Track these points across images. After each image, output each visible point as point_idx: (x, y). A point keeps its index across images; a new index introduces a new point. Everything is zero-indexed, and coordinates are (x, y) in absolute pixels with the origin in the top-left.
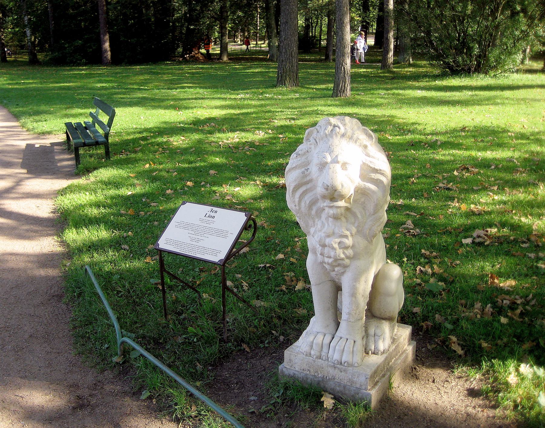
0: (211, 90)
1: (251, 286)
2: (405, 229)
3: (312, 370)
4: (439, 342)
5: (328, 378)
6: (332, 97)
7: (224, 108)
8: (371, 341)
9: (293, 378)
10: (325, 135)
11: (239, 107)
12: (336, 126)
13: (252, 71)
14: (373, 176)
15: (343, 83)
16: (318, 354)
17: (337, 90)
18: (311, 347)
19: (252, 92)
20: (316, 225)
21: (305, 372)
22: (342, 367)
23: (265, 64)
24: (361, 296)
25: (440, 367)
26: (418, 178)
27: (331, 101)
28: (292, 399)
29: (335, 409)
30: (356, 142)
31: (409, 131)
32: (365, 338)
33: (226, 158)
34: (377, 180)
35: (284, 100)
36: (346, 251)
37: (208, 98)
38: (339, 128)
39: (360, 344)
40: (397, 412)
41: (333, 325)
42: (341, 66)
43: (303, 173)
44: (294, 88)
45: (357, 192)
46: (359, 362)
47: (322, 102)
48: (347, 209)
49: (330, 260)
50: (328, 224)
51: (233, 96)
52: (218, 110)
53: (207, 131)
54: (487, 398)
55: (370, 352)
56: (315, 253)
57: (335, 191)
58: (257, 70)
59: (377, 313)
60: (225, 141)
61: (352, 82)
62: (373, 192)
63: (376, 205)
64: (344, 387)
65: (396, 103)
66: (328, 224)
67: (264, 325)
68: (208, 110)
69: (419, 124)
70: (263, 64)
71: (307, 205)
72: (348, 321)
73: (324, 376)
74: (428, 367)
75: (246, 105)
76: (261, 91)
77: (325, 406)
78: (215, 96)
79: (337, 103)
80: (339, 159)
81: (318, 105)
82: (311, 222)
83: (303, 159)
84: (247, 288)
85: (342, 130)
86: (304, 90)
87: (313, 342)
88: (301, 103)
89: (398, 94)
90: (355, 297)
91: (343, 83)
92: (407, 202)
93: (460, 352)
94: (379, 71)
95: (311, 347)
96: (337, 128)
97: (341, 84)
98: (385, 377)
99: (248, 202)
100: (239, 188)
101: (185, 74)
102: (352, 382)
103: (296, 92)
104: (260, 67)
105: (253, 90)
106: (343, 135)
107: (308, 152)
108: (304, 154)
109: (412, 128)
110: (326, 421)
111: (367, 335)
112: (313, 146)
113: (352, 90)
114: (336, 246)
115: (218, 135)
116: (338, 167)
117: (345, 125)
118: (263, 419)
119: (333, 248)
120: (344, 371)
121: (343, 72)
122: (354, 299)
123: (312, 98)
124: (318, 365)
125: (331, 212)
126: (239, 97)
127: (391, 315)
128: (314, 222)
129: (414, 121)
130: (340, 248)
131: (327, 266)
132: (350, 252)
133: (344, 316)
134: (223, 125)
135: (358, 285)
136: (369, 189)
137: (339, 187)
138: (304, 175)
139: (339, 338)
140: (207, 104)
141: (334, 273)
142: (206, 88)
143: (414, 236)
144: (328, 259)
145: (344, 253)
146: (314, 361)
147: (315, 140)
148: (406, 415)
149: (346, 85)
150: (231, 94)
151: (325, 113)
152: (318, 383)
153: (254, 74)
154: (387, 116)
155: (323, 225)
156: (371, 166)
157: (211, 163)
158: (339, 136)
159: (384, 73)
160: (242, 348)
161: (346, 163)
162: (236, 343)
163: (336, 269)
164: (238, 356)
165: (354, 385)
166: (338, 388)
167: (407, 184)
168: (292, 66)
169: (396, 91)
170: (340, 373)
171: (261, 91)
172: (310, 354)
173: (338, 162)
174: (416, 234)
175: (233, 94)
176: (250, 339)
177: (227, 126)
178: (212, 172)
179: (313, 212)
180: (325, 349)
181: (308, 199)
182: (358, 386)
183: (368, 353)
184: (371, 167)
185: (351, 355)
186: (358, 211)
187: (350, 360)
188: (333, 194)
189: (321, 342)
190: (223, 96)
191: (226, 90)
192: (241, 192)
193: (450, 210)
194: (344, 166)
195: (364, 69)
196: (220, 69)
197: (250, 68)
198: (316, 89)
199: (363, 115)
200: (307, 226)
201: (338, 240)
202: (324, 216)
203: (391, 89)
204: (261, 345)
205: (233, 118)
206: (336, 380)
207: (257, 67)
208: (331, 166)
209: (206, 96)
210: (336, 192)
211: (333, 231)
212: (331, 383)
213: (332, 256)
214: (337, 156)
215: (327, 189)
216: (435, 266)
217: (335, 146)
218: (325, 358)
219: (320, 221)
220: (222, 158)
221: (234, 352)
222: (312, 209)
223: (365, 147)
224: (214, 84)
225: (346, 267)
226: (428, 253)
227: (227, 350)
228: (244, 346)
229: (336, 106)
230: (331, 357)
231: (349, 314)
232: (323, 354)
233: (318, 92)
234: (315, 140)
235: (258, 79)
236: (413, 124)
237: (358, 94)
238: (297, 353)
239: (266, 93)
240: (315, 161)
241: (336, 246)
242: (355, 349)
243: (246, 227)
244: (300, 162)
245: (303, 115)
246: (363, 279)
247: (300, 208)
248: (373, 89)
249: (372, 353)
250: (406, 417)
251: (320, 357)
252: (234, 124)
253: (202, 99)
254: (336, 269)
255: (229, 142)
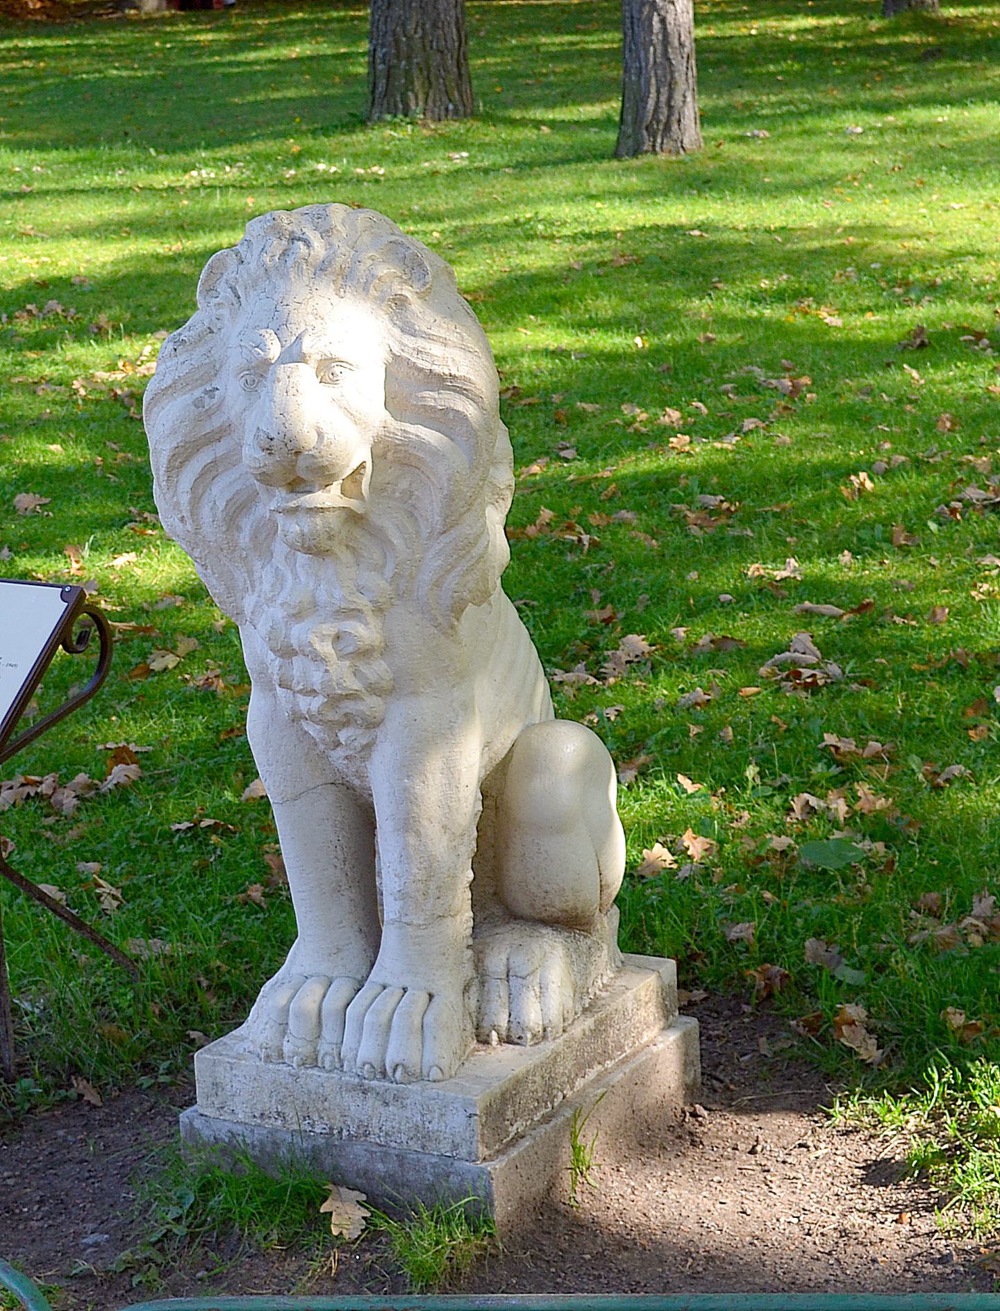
0: (65, 154)
1: (129, 894)
2: (781, 666)
3: (290, 1114)
4: (801, 1030)
5: (345, 1133)
6: (616, 155)
7: (114, 232)
8: (494, 996)
9: (230, 1149)
10: (262, 271)
11: (184, 227)
12: (299, 239)
13: (271, 53)
14: (432, 398)
15: (664, 90)
16: (306, 1050)
17: (637, 121)
18: (283, 1028)
19: (255, 157)
20: (257, 584)
21: (269, 1124)
22: (387, 1084)
23: (340, 20)
24: (438, 827)
25: (789, 1109)
26: (887, 474)
27: (607, 174)
28: (226, 1222)
29: (371, 1234)
30: (366, 289)
31: (932, 288)
32: (474, 989)
33: (92, 445)
34: (446, 411)
35: (393, 184)
36: (363, 668)
37: (47, 193)
38: (308, 243)
39: (450, 1003)
40: (594, 1243)
41: (355, 946)
42: (646, 10)
43: (198, 403)
44: (454, 127)
45: (384, 456)
46: (444, 1063)
47: (561, 181)
48: (353, 518)
49: (316, 703)
50: (296, 576)
51: (162, 180)
52: (85, 242)
53: (27, 336)
54: (923, 1179)
55: (494, 1034)
56: (268, 687)
57: (298, 453)
58: (296, 51)
59: (524, 908)
60: (102, 375)
61: (703, 85)
62: (435, 453)
63: (450, 498)
64: (401, 1158)
65: (904, 167)
66: (296, 576)
67: (162, 1016)
68: (38, 248)
69: (979, 255)
70: (330, 20)
71: (219, 515)
72: (402, 923)
73: (332, 1129)
74: (741, 1111)
75: (216, 214)
76: (296, 149)
77: (335, 1232)
78: (82, 182)
79: (634, 181)
80: (306, 346)
81: (544, 198)
82: (240, 577)
83: (197, 356)
84: (115, 903)
85: (319, 247)
86: (492, 133)
87: (286, 1009)
88: (465, 196)
89: (928, 129)
90: (418, 834)
91: (664, 90)
92: (818, 567)
93: (870, 1051)
94: (875, 24)
95: (283, 1028)
96: (301, 244)
97: (653, 95)
98: (552, 1124)
99: (161, 607)
100: (132, 556)
101: (845, 49)
102: (425, 1137)
103: (459, 145)
104: (314, 34)
105: (259, 146)
106: (322, 268)
107: (212, 332)
108: (201, 337)
109: (948, 274)
110: (335, 1280)
111: (481, 975)
112: (225, 312)
113: (706, 119)
114: (326, 648)
115: (74, 351)
116: (304, 375)
117: (326, 233)
118: (120, 1293)
119: (317, 658)
120: (396, 1098)
121: (657, 38)
122: (412, 840)
123: (523, 168)
124: (310, 1092)
125: (294, 527)
126: (193, 177)
127: (571, 904)
128: (250, 572)
129: (960, 242)
130: (340, 658)
131: (312, 729)
132: (378, 669)
133: (390, 908)
134: (99, 309)
135: (419, 789)
136: (421, 444)
137: (309, 439)
138: (202, 410)
139: (379, 988)
140: (41, 220)
141: (340, 752)
142: (41, 146)
143: (812, 688)
144: (308, 699)
145: (356, 673)
146: (296, 1077)
147: (233, 289)
148: (626, 1249)
149: (678, 98)
150: (154, 168)
151: (566, 231)
152: (315, 1155)
153: (282, 71)
154: (846, 229)
155: (278, 576)
156: (421, 364)
157: (27, 465)
158: (308, 272)
159: (895, 31)
160: (72, 1093)
161: (332, 360)
162: (48, 1079)
163: (343, 736)
164: (58, 1120)
165: (431, 1146)
166: (380, 1166)
167: (834, 499)
168: (434, 26)
169: (921, 115)
170: (382, 1109)
171: (294, 146)
172: (281, 1055)
173: (302, 358)
174: (821, 682)
175: (165, 167)
176: (103, 1060)
177: (116, 311)
178: (25, 500)
179: (244, 538)
180: (329, 1034)
181: (220, 493)
182: (446, 1149)
183: (486, 1042)
184: (421, 370)
185: (415, 1041)
186: (389, 522)
187: (413, 1059)
188: (293, 466)
189: (314, 1007)
190: (117, 178)
191: (132, 153)
192: (138, 572)
193: (985, 587)
194: (328, 369)
195: (807, 15)
196: (122, 53)
197: (268, 38)
198: (553, 124)
199: (735, 229)
200: (230, 589)
201: (330, 629)
202: (280, 548)
203: (900, 105)
204: (145, 1081)
205: (148, 276)
206: (372, 1138)
207: (300, 37)
208: (282, 371)
209: (36, 185)
210: (300, 457)
211: (314, 596)
212: (358, 1149)
213: (317, 687)
214: (299, 338)
215: (269, 450)
216: (863, 789)
217: (293, 306)
218: (332, 1062)
219: (268, 568)
220: (76, 441)
221: (42, 1109)
222: (239, 529)
223: (400, 303)
224: (81, 127)
225: (372, 724)
226: (848, 745)
227: (15, 1105)
228: (80, 1085)
229: (627, 195)
230: (350, 1056)
231: (403, 895)
232: (324, 1048)
233: (559, 139)
234: (233, 289)
235: (291, 93)
236: (954, 256)
237: (742, 139)
238: (239, 1057)
239: (316, 155)
240: (235, 360)
241: (326, 648)
242: (429, 1019)
243: (62, 636)
244: (185, 369)
245: (463, 245)
246: (434, 766)
247: (198, 528)
248: (819, 110)
249: (501, 1041)
250: (626, 1254)
251: (313, 1061)
252: (151, 300)
253: (20, 196)
254: (343, 736)
255: (119, 376)
